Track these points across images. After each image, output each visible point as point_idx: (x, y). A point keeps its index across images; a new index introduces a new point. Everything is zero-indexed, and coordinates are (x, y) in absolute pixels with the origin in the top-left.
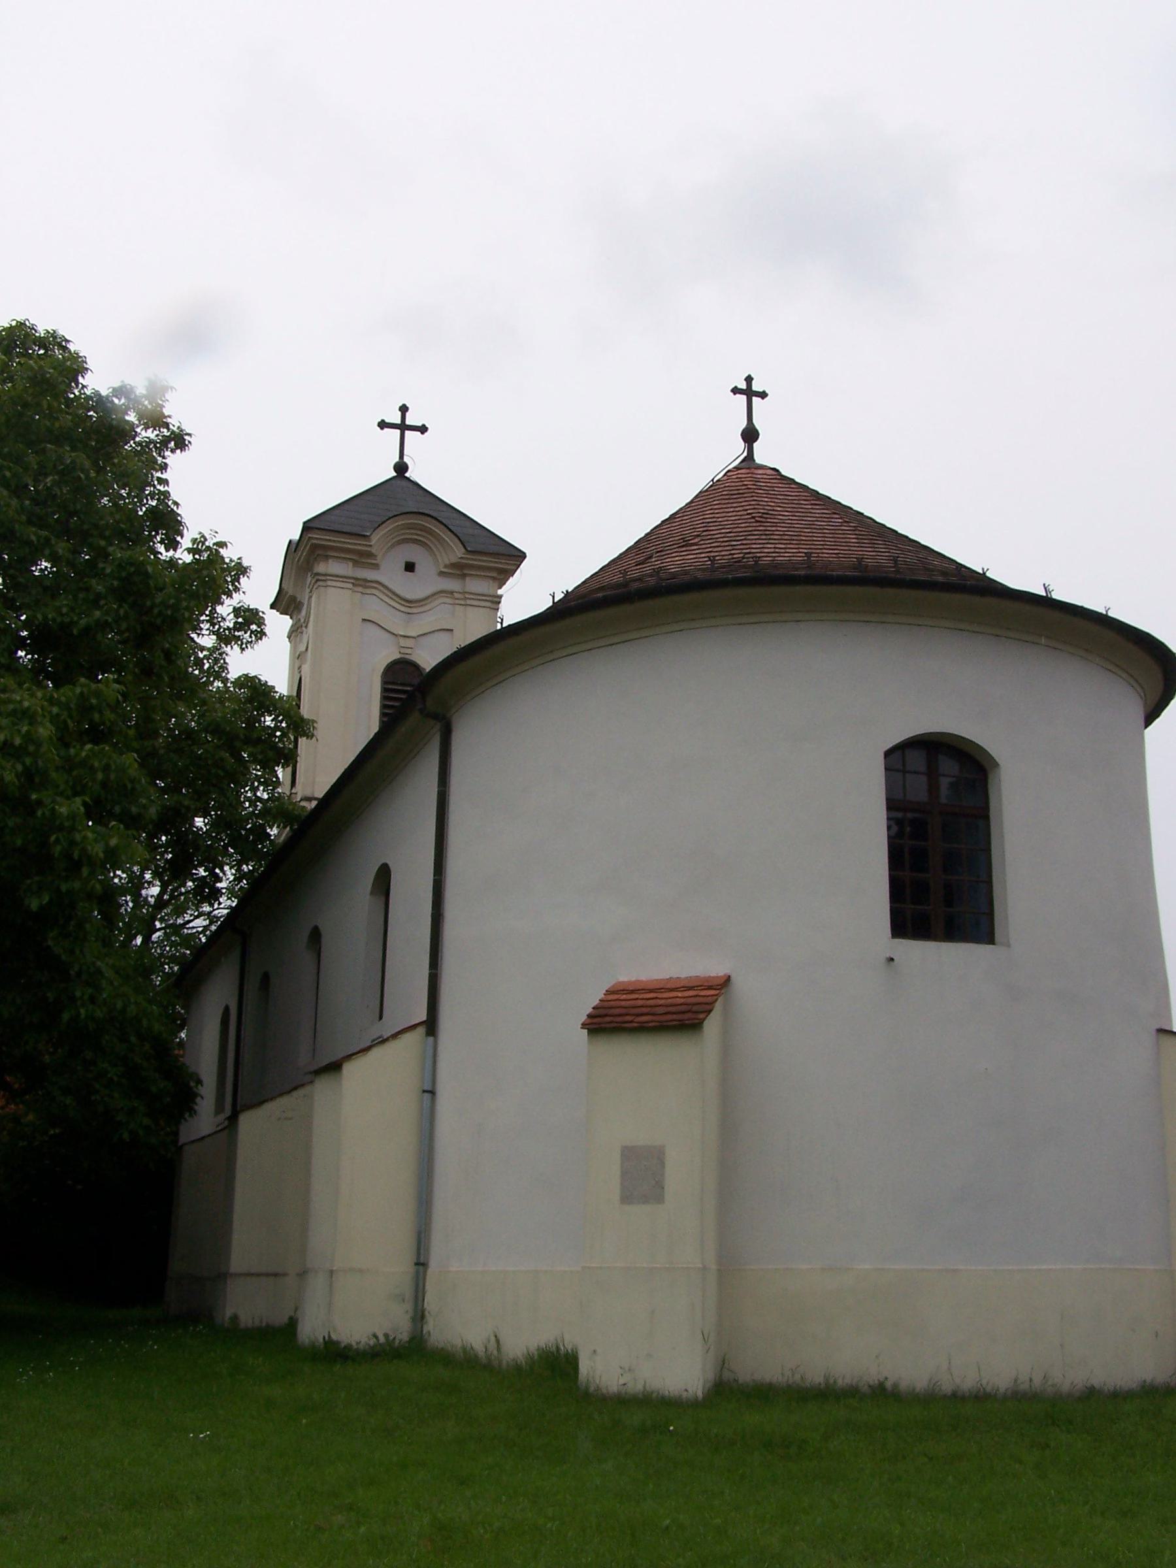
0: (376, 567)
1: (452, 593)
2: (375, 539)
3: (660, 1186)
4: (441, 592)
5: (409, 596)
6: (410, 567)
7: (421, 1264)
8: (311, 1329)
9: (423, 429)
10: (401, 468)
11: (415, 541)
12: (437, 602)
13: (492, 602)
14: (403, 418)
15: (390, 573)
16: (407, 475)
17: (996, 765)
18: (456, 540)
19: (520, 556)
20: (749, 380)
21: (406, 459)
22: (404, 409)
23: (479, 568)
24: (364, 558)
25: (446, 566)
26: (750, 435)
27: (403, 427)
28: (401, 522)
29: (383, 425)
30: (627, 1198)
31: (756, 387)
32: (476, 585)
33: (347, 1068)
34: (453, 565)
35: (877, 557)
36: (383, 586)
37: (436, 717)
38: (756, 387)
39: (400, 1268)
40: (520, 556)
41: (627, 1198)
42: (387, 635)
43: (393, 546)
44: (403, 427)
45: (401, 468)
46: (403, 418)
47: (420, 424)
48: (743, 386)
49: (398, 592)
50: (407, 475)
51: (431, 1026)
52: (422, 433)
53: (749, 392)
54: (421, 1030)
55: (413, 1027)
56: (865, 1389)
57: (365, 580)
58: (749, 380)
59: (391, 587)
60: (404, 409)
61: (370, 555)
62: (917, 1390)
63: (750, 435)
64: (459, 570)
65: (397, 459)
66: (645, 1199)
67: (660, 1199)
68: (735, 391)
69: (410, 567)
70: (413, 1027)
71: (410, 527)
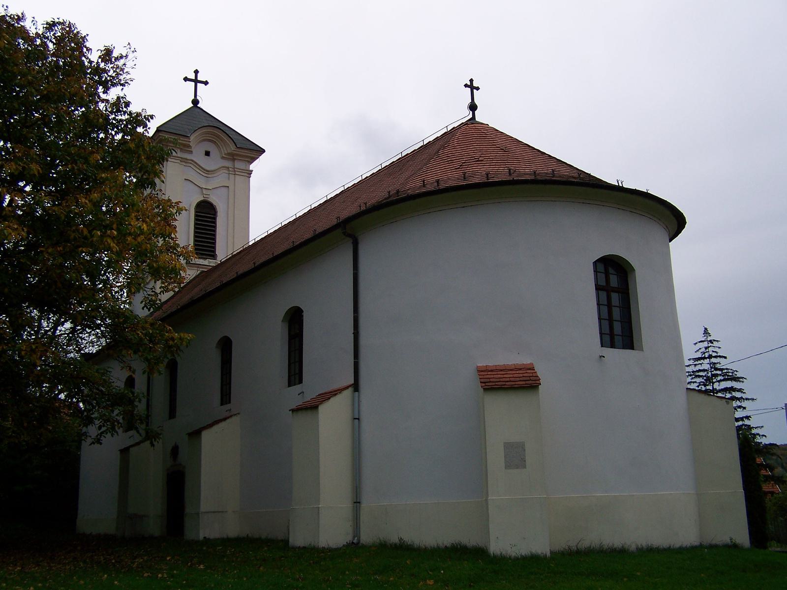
0: (191, 152)
1: (228, 168)
2: (192, 138)
3: (524, 460)
4: (223, 167)
5: (208, 169)
6: (207, 154)
7: (357, 503)
8: (298, 539)
9: (206, 83)
10: (195, 102)
11: (210, 141)
12: (221, 172)
13: (248, 174)
14: (196, 76)
15: (197, 155)
16: (198, 106)
17: (633, 270)
18: (231, 141)
19: (264, 151)
20: (471, 81)
21: (198, 98)
22: (196, 72)
23: (240, 156)
24: (186, 148)
25: (225, 154)
26: (473, 107)
27: (196, 81)
28: (205, 130)
29: (186, 79)
30: (508, 466)
31: (475, 85)
32: (239, 165)
33: (322, 408)
34: (229, 154)
35: (544, 170)
36: (196, 163)
37: (350, 236)
38: (475, 85)
39: (346, 505)
40: (206, 151)
41: (508, 466)
42: (197, 188)
43: (200, 142)
44: (196, 81)
45: (195, 102)
46: (196, 76)
47: (205, 81)
48: (469, 84)
49: (201, 165)
50: (198, 106)
51: (356, 387)
52: (206, 85)
53: (471, 87)
54: (350, 390)
55: (347, 388)
56: (721, 545)
57: (186, 159)
58: (471, 81)
59: (198, 162)
60: (196, 72)
61: (189, 146)
62: (615, 546)
63: (473, 107)
64: (232, 157)
65: (193, 98)
66: (517, 467)
67: (525, 467)
68: (466, 86)
69: (207, 154)
70: (347, 388)
71: (208, 133)
